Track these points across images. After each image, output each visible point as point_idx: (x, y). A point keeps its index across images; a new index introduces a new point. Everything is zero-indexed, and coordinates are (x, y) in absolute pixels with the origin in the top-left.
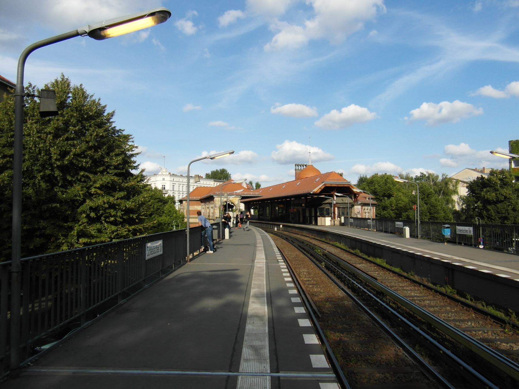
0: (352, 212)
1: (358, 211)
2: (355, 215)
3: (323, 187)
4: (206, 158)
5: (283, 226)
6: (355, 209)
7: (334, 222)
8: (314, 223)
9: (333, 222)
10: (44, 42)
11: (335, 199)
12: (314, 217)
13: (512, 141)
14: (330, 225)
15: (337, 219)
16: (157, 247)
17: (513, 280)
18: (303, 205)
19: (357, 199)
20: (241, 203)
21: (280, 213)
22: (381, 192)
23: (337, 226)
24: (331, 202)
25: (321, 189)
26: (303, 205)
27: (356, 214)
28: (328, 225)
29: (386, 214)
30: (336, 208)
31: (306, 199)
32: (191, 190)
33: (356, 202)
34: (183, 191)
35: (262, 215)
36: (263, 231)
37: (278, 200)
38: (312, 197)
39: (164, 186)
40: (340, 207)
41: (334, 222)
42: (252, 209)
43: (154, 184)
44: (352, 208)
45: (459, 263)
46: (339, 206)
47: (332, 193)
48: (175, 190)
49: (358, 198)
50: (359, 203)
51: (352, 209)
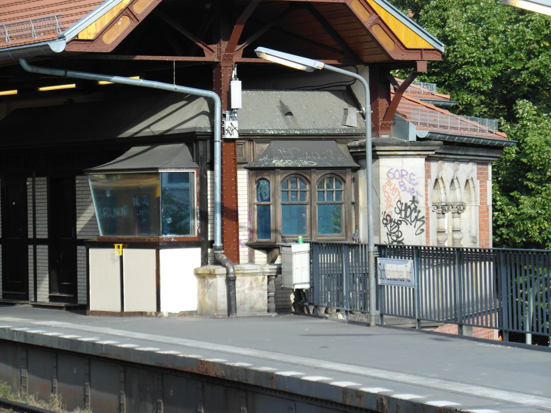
0: (355, 204)
1: (407, 199)
2: (384, 230)
6: (383, 181)
7: (230, 281)
9: (220, 283)
11: (237, 100)
12: (43, 251)
14: (194, 307)
15: (251, 260)
19: (393, 106)
22: (488, 64)
23: (254, 316)
24: (203, 123)
27: (388, 220)
28: (177, 310)
29: (531, 218)
30: (242, 176)
33: (386, 128)
40: (273, 169)
41: (230, 281)
44: (355, 170)
46: (264, 162)
47: (210, 57)
49: (402, 107)
50: (414, 133)
51: (355, 180)
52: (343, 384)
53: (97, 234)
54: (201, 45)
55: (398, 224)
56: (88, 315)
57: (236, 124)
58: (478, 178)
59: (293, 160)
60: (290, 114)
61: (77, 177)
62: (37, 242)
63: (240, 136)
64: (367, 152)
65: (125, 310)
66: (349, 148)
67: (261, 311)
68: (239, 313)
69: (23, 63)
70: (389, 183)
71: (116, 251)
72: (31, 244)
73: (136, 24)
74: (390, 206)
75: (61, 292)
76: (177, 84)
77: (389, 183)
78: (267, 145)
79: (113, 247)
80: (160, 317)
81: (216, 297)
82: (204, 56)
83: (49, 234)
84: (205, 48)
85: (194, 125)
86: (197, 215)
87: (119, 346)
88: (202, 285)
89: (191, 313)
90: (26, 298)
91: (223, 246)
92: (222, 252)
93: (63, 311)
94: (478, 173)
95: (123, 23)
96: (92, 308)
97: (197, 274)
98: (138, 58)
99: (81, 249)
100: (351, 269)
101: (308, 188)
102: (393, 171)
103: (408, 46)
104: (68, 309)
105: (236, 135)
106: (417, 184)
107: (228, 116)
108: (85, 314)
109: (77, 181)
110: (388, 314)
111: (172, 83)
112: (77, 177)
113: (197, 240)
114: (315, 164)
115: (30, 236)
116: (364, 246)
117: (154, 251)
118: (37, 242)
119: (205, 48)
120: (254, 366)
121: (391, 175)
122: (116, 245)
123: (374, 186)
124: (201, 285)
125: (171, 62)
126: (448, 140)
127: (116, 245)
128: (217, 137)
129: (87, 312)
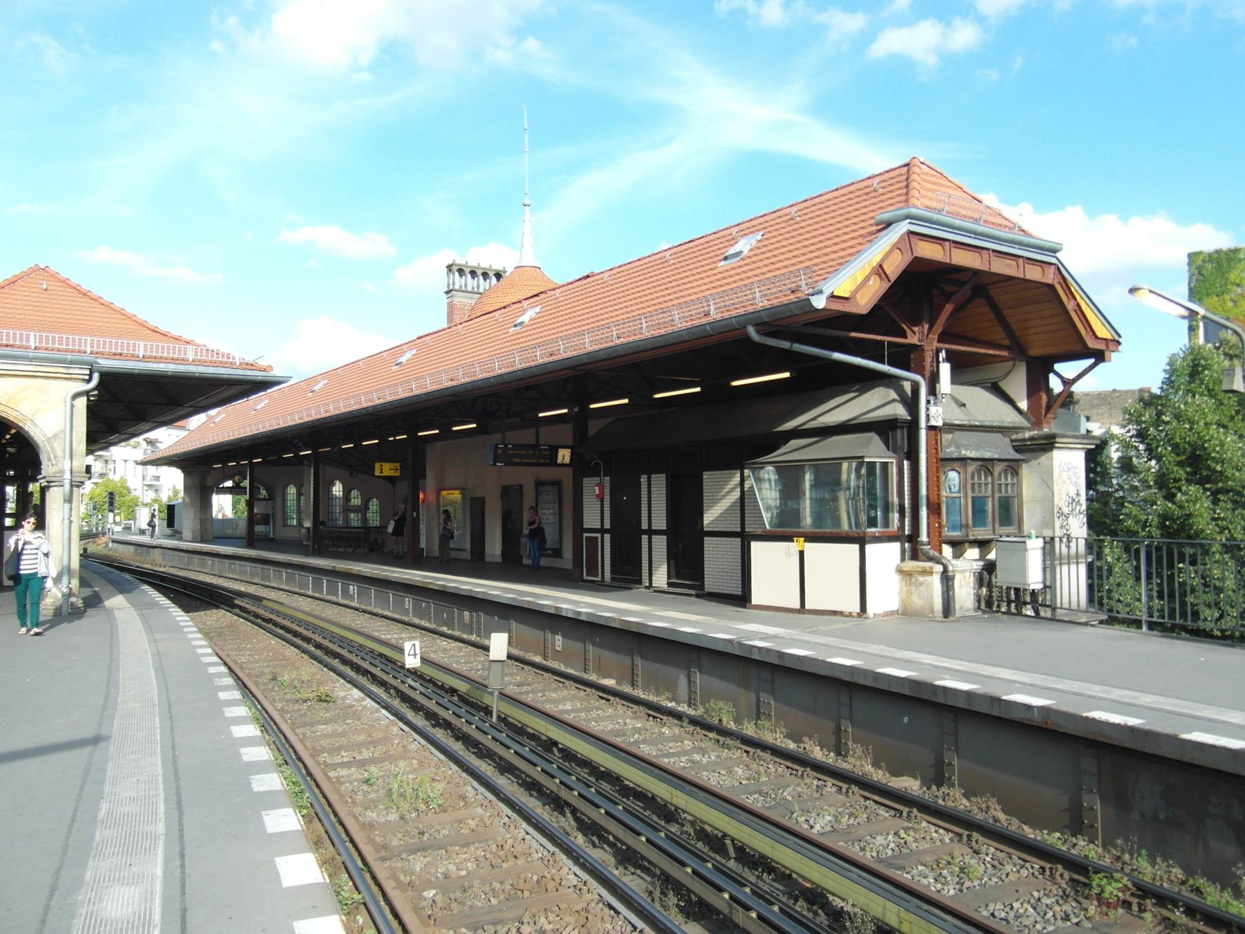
5: (1179, 563)
8: (661, 577)
12: (660, 543)
13: (1200, 253)
16: (1023, 569)
18: (564, 455)
21: (356, 509)
24: (900, 411)
26: (564, 455)
31: (581, 419)
35: (265, 520)
37: (383, 441)
38: (641, 400)
47: (912, 339)
53: (763, 526)
54: (905, 327)
55: (1067, 518)
56: (750, 609)
57: (940, 410)
59: (977, 450)
60: (964, 405)
61: (704, 473)
64: (78, 539)
65: (808, 606)
66: (1012, 441)
67: (968, 610)
68: (958, 613)
69: (751, 331)
71: (794, 547)
72: (645, 534)
73: (886, 285)
74: (1061, 499)
75: (677, 578)
76: (889, 364)
78: (951, 435)
79: (793, 541)
80: (866, 618)
81: (932, 597)
82: (906, 337)
83: (667, 526)
84: (908, 330)
85: (891, 412)
86: (896, 508)
88: (906, 582)
89: (892, 613)
90: (640, 582)
91: (929, 542)
92: (929, 547)
93: (693, 599)
95: (874, 283)
96: (756, 599)
97: (900, 571)
98: (854, 334)
101: (990, 479)
102: (1063, 464)
103: (1099, 336)
104: (698, 596)
105: (940, 423)
107: (932, 402)
108: (745, 607)
109: (704, 477)
110: (1061, 608)
111: (884, 363)
112: (704, 473)
113: (896, 534)
114: (997, 456)
115: (645, 526)
117: (856, 547)
119: (908, 330)
121: (1061, 468)
122: (795, 539)
123: (1045, 479)
124: (904, 583)
125: (882, 342)
126: (734, 471)
127: (795, 539)
128: (923, 424)
129: (748, 605)
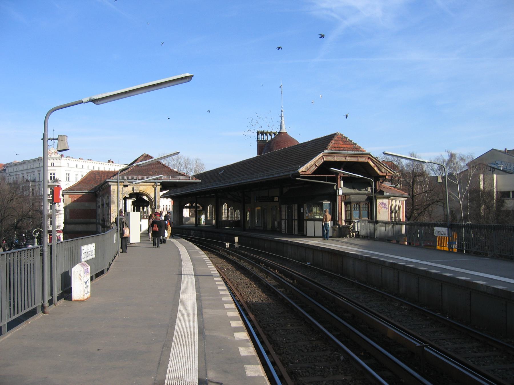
3: (321, 162)
4: (82, 102)
10: (46, 175)
12: (296, 222)
17: (473, 283)
18: (276, 199)
20: (160, 199)
25: (316, 166)
32: (272, 138)
34: (118, 185)
36: (197, 248)
39: (54, 174)
42: (187, 207)
43: (38, 171)
45: (503, 286)
48: (117, 181)
52: (391, 261)
58: (401, 204)
62: (295, 220)
63: (342, 194)
70: (379, 206)
76: (327, 182)
77: (379, 206)
87: (371, 257)
94: (401, 203)
99: (305, 221)
100: (453, 243)
106: (386, 206)
115: (293, 218)
116: (52, 164)
117: (313, 222)
118: (295, 220)
120: (371, 256)
